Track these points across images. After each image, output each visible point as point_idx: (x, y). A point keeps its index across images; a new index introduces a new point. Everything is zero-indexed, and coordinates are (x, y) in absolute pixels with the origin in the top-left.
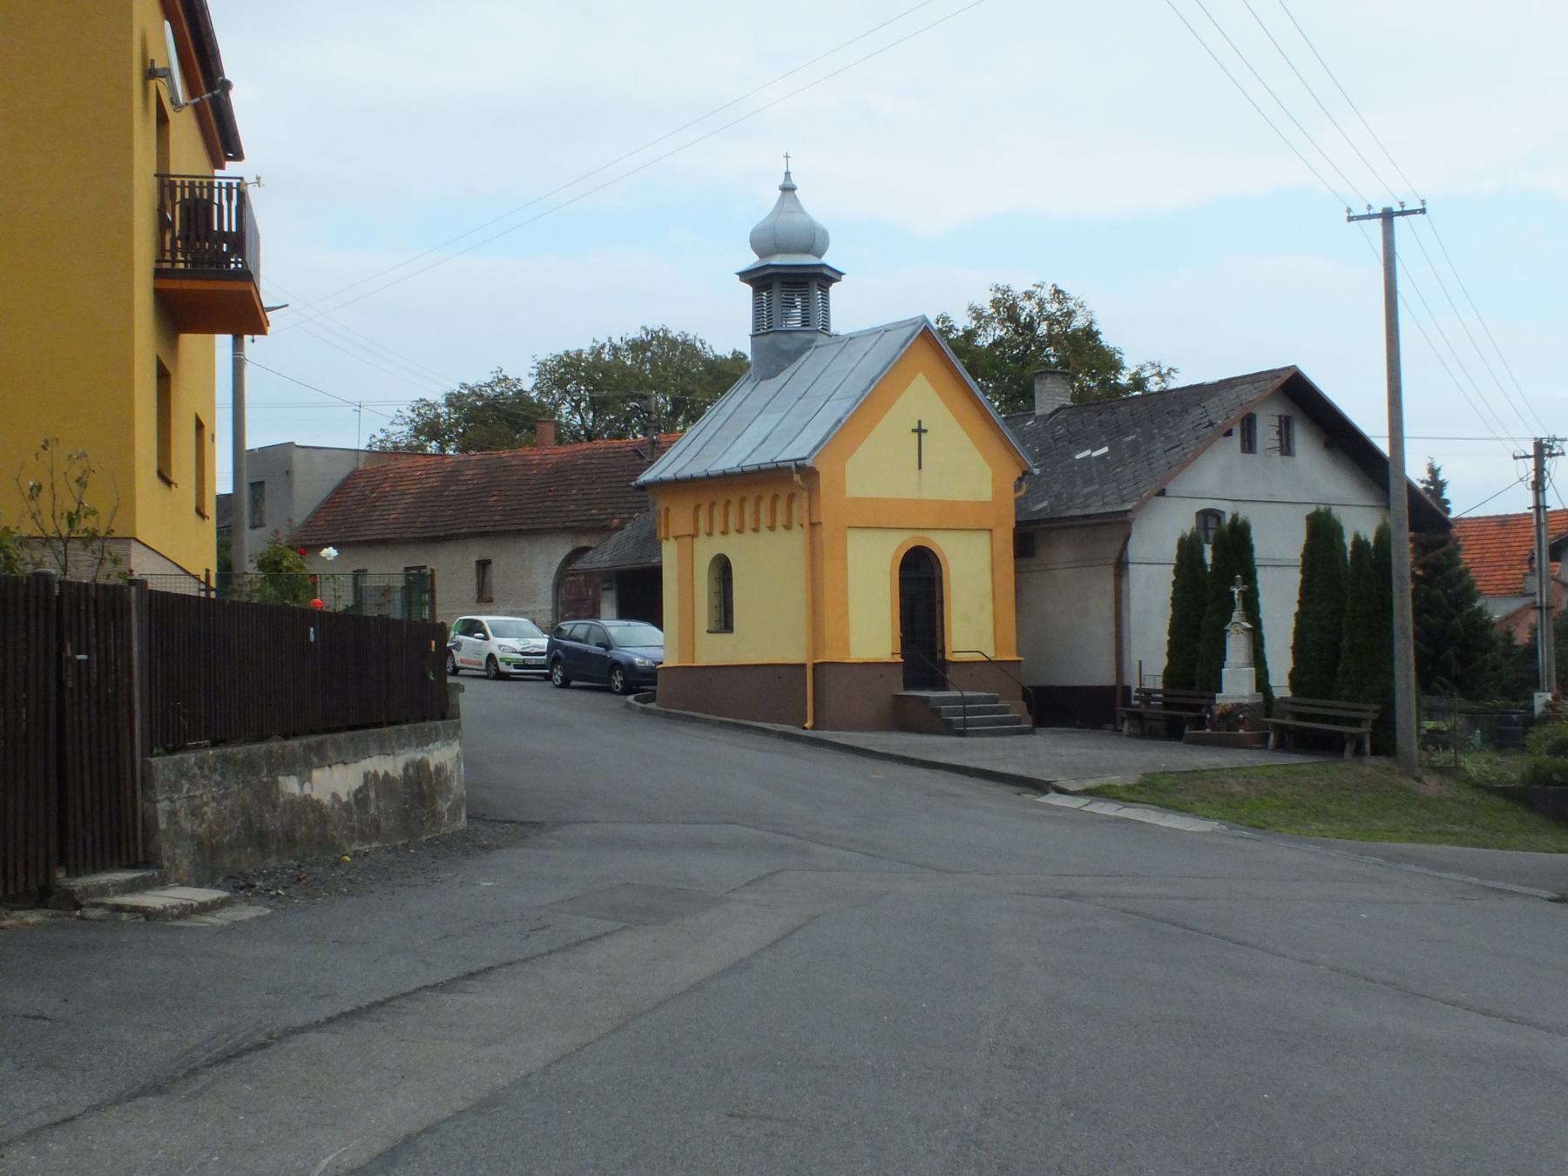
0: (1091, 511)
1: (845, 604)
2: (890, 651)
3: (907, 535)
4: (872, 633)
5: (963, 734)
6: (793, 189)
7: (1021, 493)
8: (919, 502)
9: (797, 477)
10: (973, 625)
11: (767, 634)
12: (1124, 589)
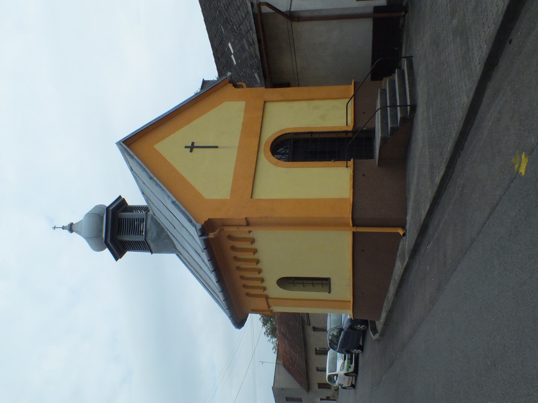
0: (255, 36)
1: (308, 201)
2: (345, 169)
3: (262, 156)
4: (331, 182)
5: (414, 108)
6: (71, 225)
7: (244, 85)
8: (240, 147)
9: (211, 235)
10: (331, 114)
11: (333, 255)
12: (307, 14)
